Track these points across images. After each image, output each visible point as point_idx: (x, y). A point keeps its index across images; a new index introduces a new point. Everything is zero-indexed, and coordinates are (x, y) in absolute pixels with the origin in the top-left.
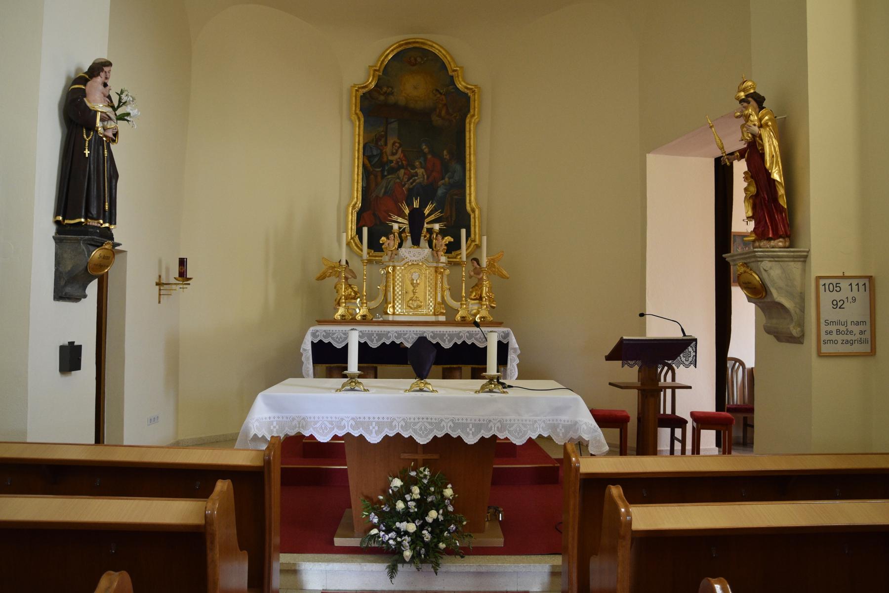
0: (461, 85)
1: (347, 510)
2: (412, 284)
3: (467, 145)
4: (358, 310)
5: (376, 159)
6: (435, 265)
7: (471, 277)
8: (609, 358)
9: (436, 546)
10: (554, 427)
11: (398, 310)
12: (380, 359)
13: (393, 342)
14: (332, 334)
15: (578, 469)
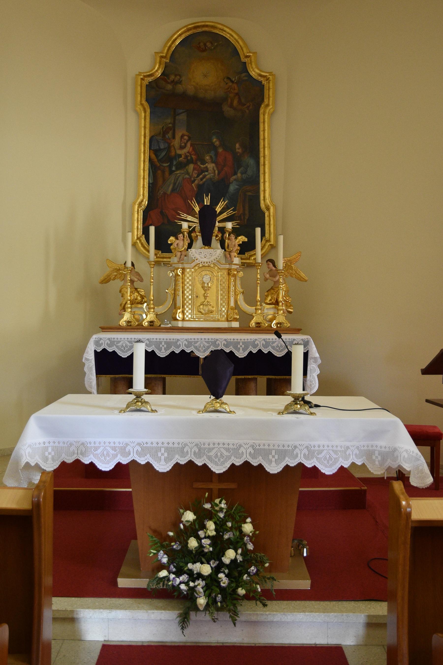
0: (254, 72)
1: (133, 541)
2: (203, 287)
3: (261, 137)
4: (144, 316)
5: (163, 154)
6: (227, 266)
7: (266, 279)
8: (426, 371)
9: (234, 591)
10: (369, 454)
11: (187, 316)
12: (168, 370)
13: (183, 351)
14: (118, 342)
15: (409, 515)
